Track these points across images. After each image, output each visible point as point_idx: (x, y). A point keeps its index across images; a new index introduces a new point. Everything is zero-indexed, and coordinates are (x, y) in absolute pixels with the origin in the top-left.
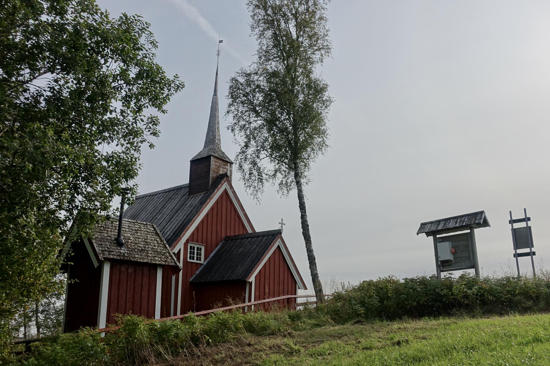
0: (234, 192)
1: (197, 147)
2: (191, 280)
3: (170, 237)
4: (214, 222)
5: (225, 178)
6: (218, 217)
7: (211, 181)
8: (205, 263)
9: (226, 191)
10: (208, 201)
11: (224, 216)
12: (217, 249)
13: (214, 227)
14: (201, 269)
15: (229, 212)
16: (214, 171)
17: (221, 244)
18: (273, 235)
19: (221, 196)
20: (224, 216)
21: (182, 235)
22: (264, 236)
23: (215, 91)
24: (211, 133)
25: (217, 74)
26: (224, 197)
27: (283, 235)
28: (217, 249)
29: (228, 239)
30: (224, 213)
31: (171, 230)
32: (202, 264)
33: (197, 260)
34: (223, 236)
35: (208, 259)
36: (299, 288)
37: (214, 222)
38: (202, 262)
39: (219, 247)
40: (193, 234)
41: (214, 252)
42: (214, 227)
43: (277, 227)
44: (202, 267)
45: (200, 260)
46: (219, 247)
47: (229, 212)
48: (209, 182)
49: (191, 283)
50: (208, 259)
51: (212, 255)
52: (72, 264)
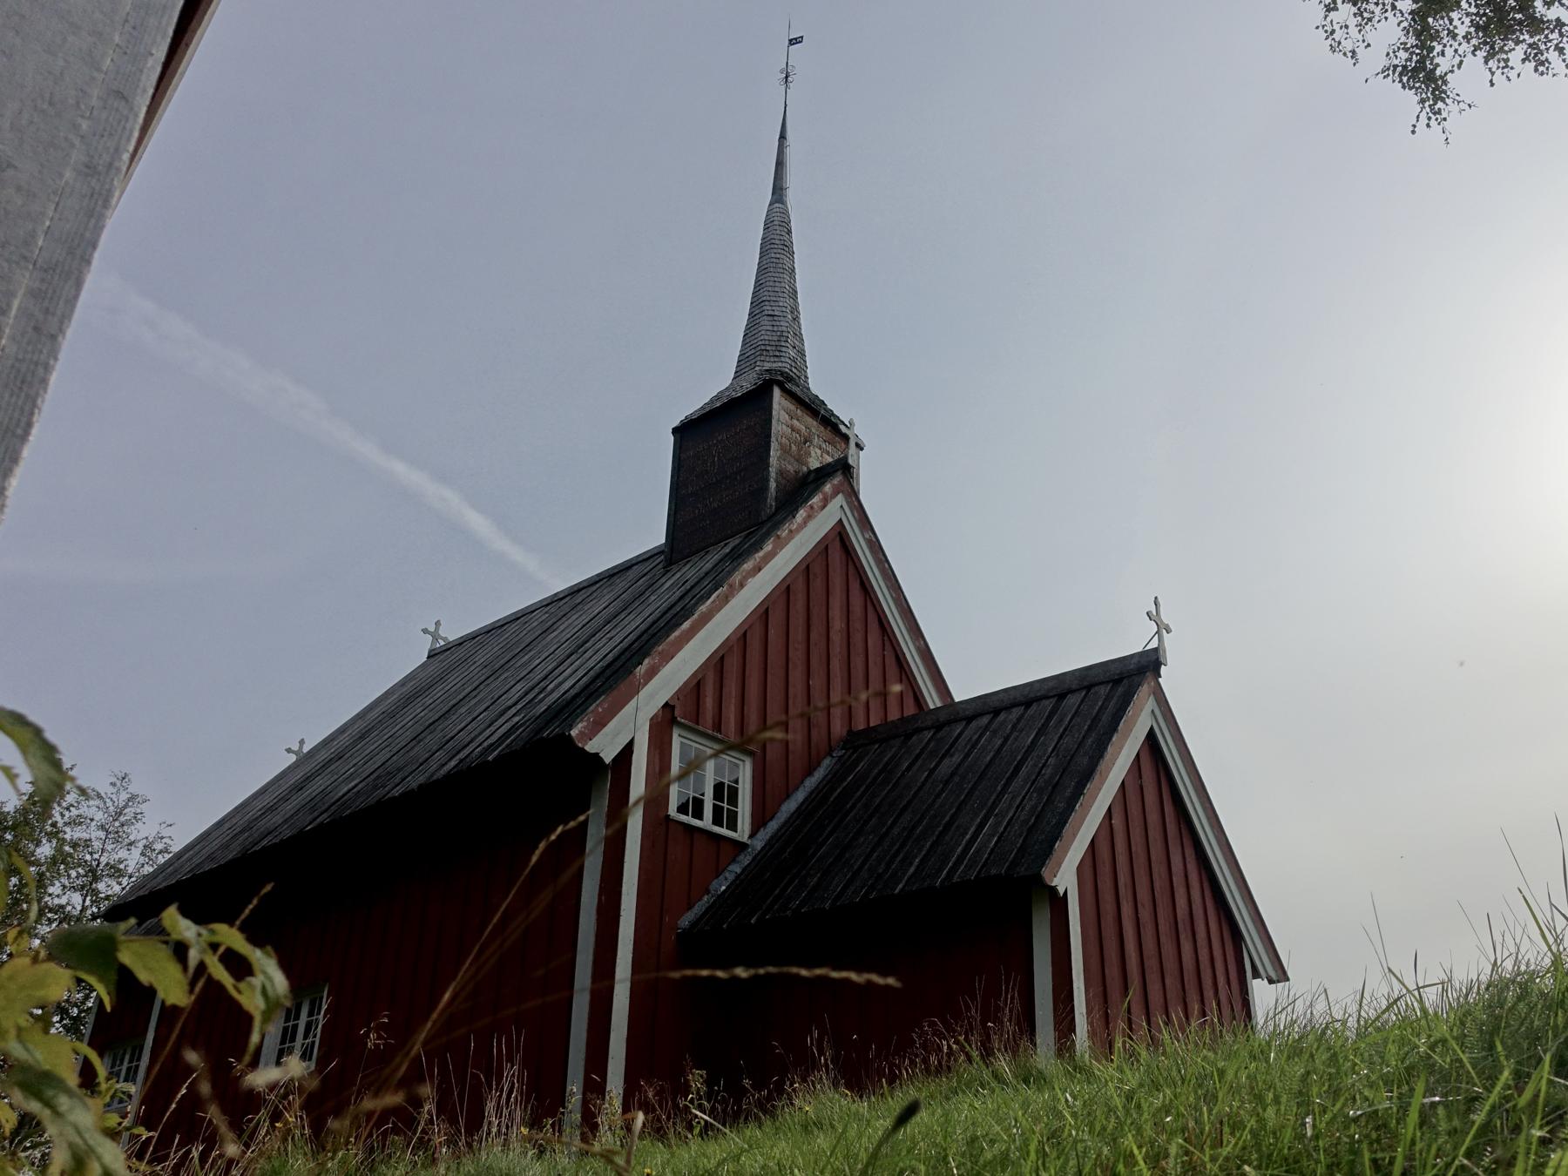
0: (876, 547)
1: (712, 376)
2: (685, 921)
3: (573, 692)
4: (797, 655)
5: (838, 479)
6: (814, 636)
7: (773, 485)
8: (758, 844)
9: (840, 532)
10: (768, 547)
11: (837, 638)
12: (811, 783)
13: (797, 676)
14: (736, 868)
15: (857, 625)
16: (785, 451)
17: (827, 762)
18: (1117, 682)
19: (823, 549)
20: (837, 638)
21: (641, 670)
22: (1062, 696)
23: (779, 191)
24: (765, 321)
25: (783, 137)
26: (836, 556)
27: (1168, 678)
28: (811, 783)
29: (856, 741)
30: (837, 624)
31: (587, 655)
32: (741, 847)
33: (717, 820)
34: (838, 729)
35: (773, 826)
36: (1256, 975)
37: (797, 655)
38: (743, 832)
39: (819, 774)
40: (694, 688)
41: (800, 796)
42: (797, 676)
43: (1129, 642)
44: (745, 859)
45: (733, 826)
46: (819, 774)
47: (857, 625)
48: (765, 488)
49: (687, 933)
50: (773, 826)
51: (790, 806)
52: (268, 888)
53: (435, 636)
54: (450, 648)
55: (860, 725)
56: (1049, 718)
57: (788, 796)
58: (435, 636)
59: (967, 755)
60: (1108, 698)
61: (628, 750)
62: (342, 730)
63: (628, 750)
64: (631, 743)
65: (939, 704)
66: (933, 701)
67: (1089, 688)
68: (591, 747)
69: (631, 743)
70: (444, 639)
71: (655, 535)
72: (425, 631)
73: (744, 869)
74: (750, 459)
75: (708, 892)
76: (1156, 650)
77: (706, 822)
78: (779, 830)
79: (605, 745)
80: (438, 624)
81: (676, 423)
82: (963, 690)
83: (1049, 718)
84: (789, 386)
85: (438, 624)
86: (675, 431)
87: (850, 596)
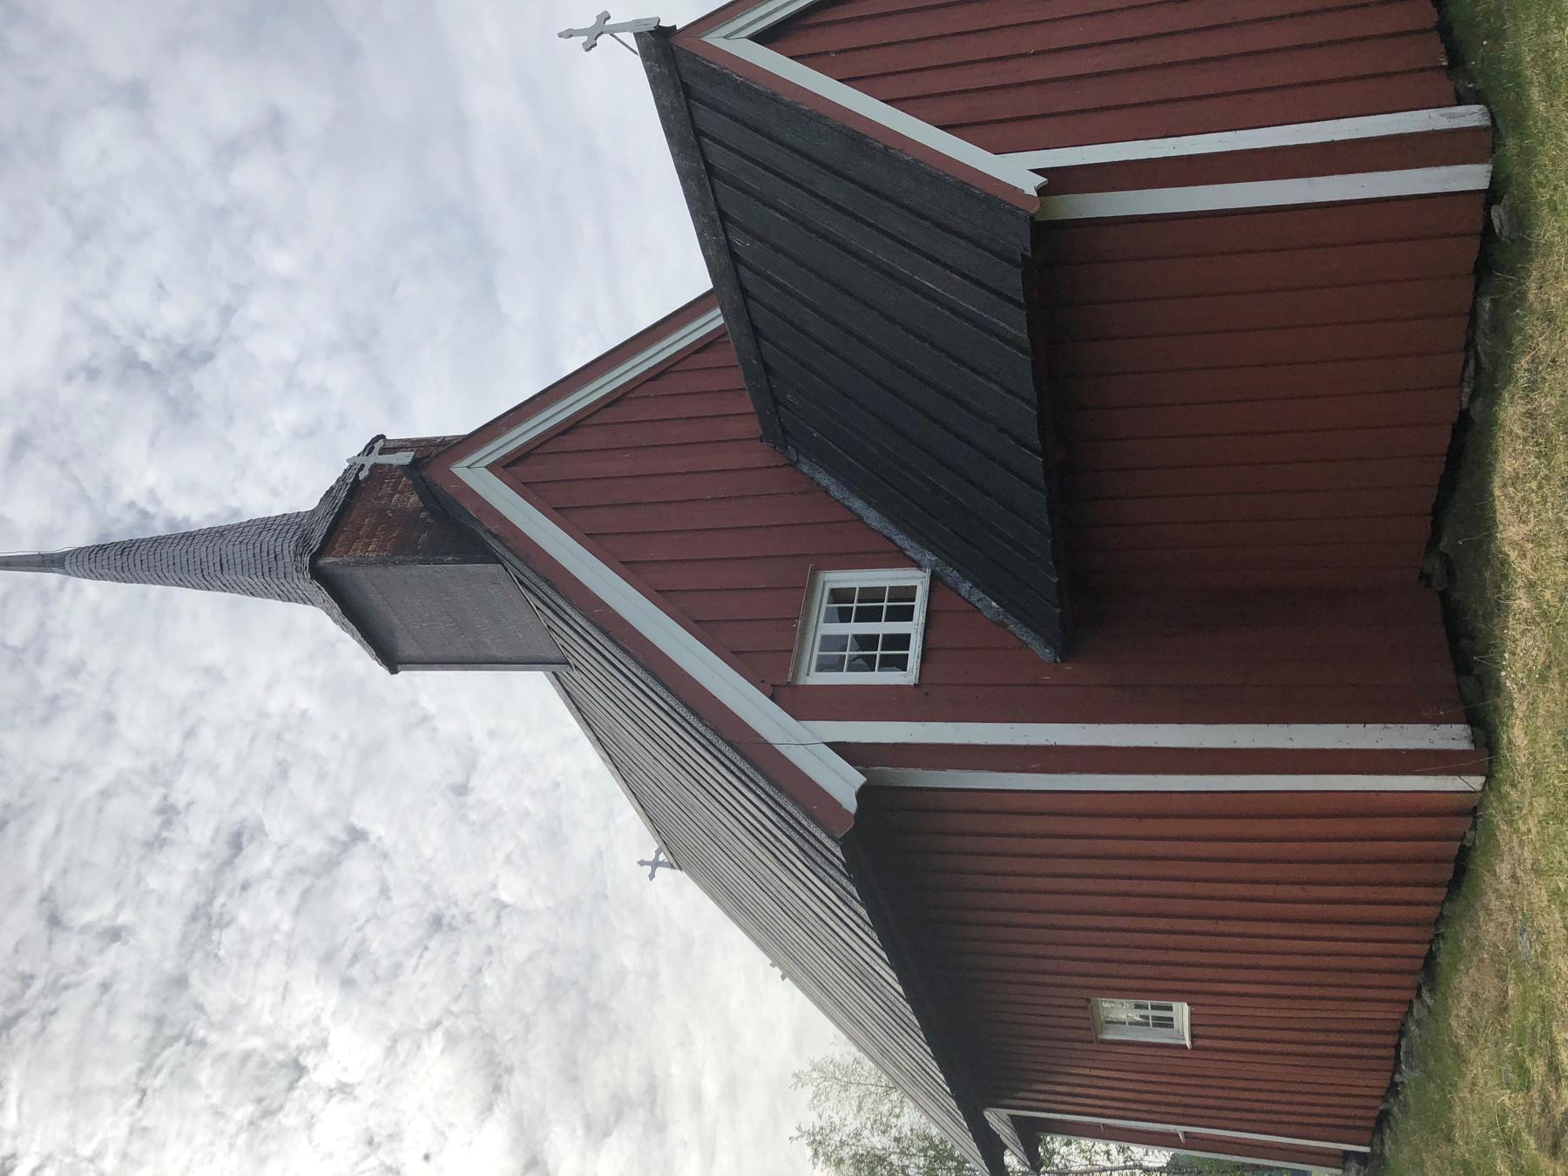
1: (309, 629)
8: (930, 557)
18: (687, 91)
19: (528, 490)
32: (935, 578)
33: (907, 614)
41: (857, 504)
44: (952, 575)
45: (909, 593)
46: (824, 479)
50: (901, 540)
51: (873, 518)
53: (655, 864)
54: (666, 845)
55: (755, 426)
56: (746, 191)
57: (861, 519)
58: (655, 864)
59: (803, 301)
60: (714, 107)
61: (843, 749)
62: (502, 519)
63: (843, 749)
64: (836, 747)
65: (718, 311)
66: (713, 320)
67: (698, 133)
68: (851, 805)
69: (836, 747)
70: (658, 853)
71: (534, 686)
72: (652, 876)
73: (965, 578)
74: (396, 548)
75: (1001, 624)
76: (637, 36)
77: (913, 628)
78: (904, 531)
79: (843, 784)
80: (642, 863)
81: (382, 671)
82: (695, 279)
83: (746, 191)
84: (316, 544)
85: (642, 863)
86: (394, 671)
87: (590, 442)
